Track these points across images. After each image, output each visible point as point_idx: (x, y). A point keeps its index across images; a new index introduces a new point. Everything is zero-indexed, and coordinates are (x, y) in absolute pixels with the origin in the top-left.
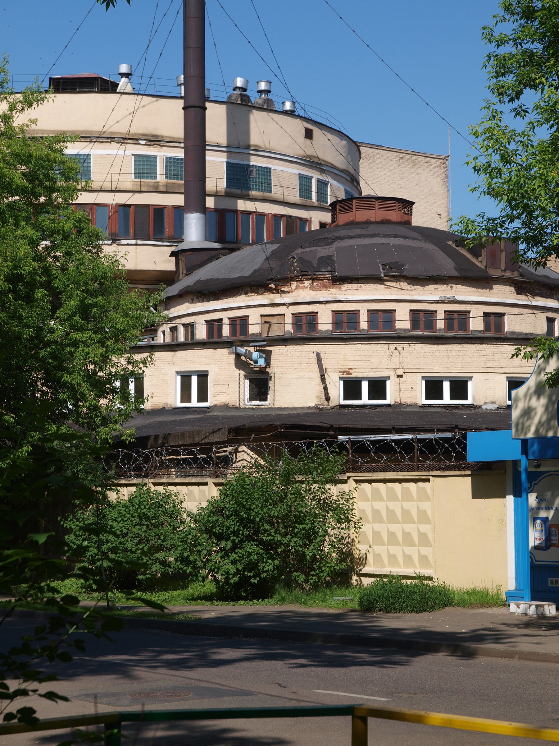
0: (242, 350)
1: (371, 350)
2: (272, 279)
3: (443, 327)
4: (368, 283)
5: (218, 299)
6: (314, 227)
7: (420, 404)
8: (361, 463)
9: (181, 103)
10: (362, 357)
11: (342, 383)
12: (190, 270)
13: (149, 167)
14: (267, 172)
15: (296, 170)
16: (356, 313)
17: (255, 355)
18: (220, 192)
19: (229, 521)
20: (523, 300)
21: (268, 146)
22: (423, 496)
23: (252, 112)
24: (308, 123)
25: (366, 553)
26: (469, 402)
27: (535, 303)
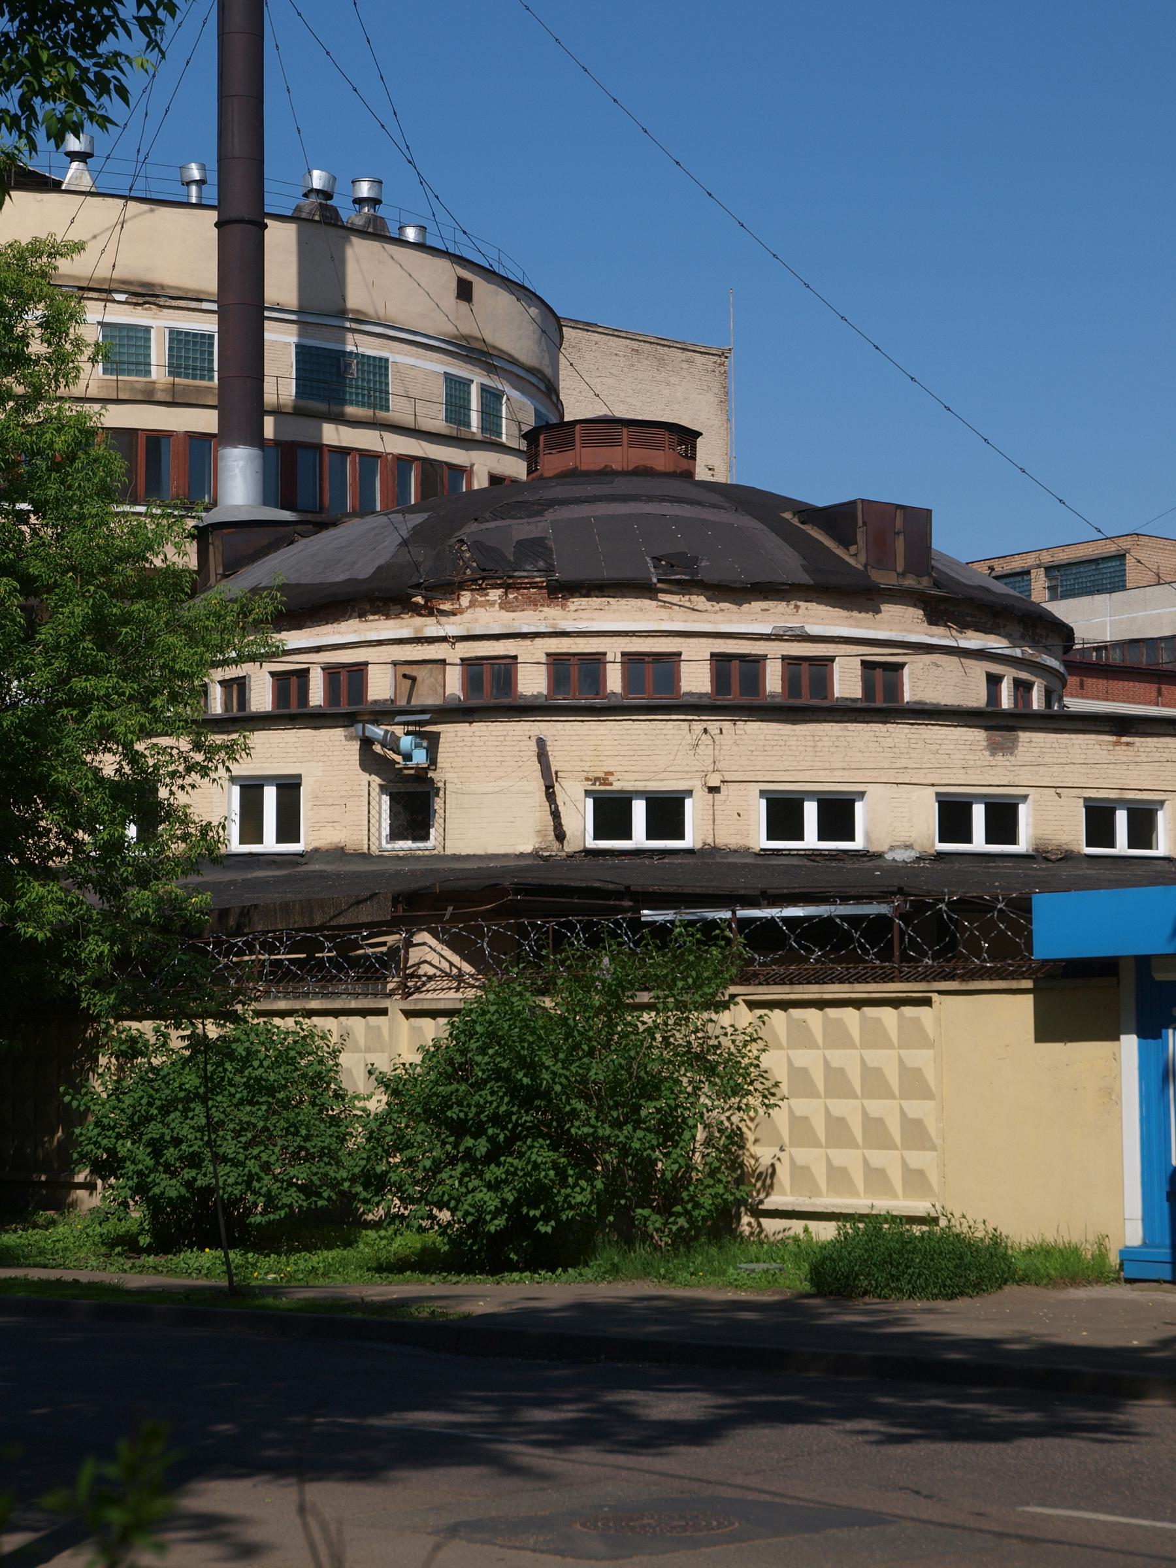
0: (378, 731)
1: (654, 732)
2: (418, 586)
3: (780, 690)
4: (623, 596)
5: (300, 627)
6: (479, 483)
7: (757, 850)
8: (760, 964)
9: (213, 216)
10: (635, 747)
11: (590, 802)
12: (231, 568)
13: (133, 350)
14: (380, 367)
15: (437, 365)
16: (598, 659)
17: (406, 742)
18: (285, 406)
19: (483, 1093)
20: (939, 636)
21: (381, 312)
22: (914, 1037)
23: (350, 241)
24: (464, 267)
25: (773, 1165)
26: (858, 844)
27: (964, 644)
